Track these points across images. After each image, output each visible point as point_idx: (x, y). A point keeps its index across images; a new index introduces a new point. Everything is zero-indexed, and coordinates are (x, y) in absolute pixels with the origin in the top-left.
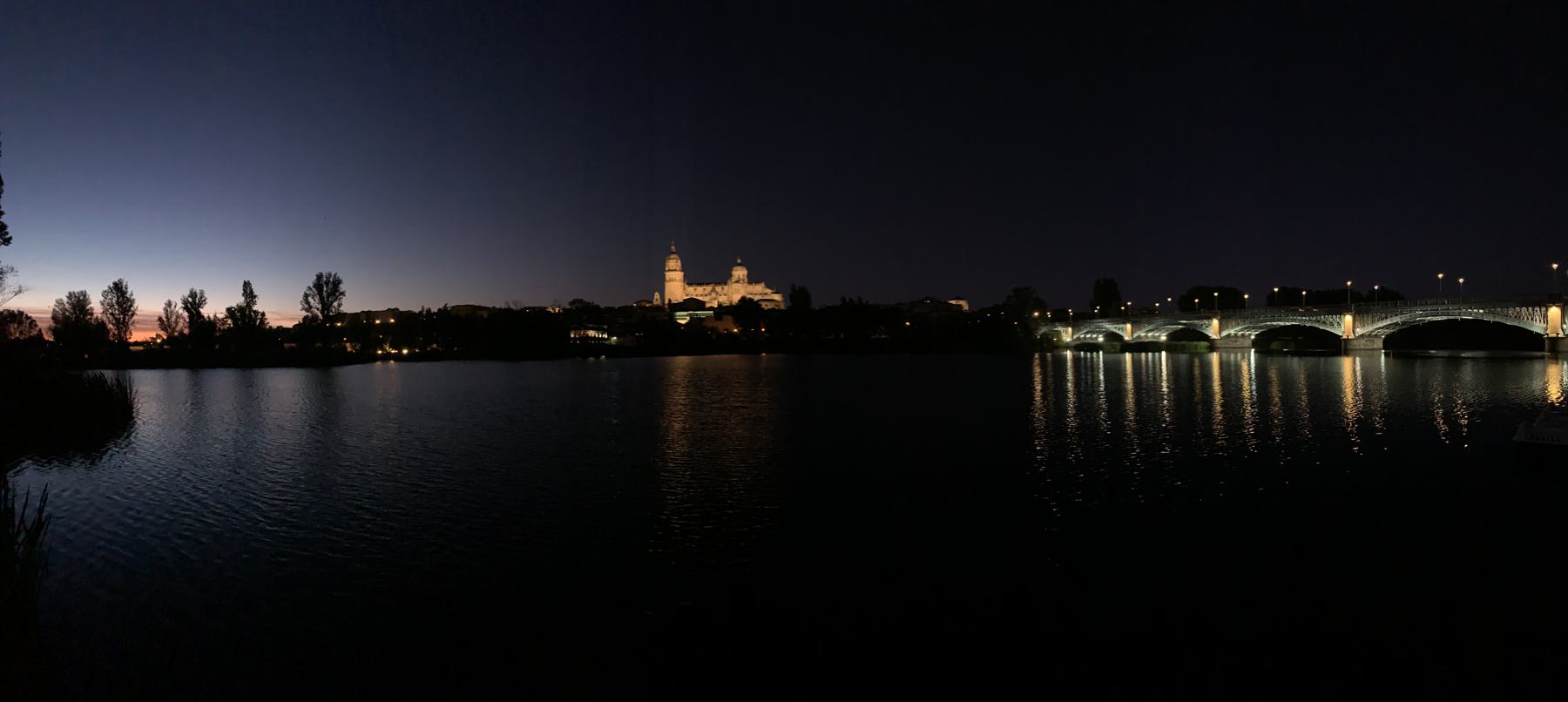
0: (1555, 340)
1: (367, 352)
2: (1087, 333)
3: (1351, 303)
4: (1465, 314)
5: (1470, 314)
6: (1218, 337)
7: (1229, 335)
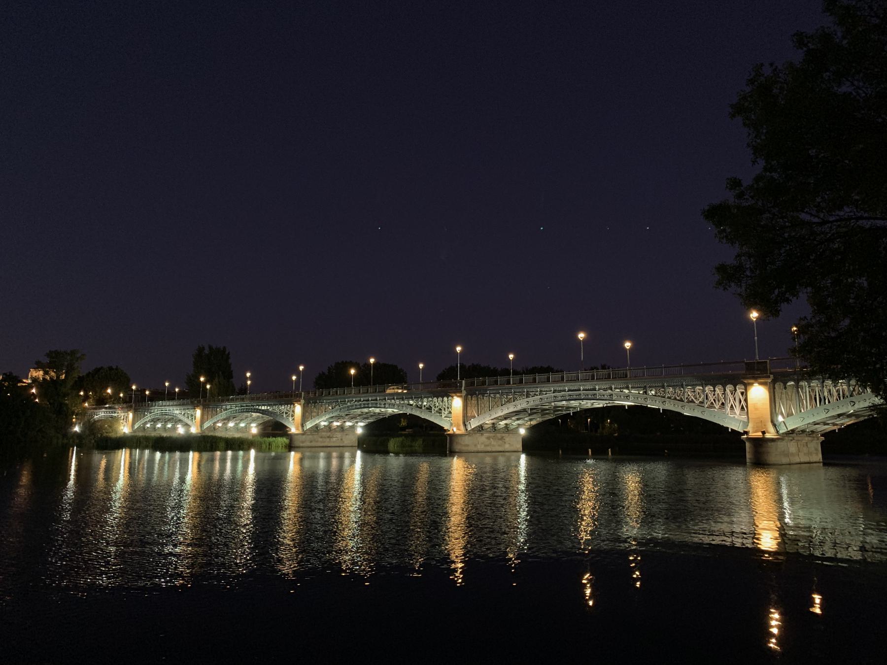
0: (760, 443)
1: (716, 217)
2: (228, 419)
3: (462, 379)
4: (619, 398)
5: (627, 397)
6: (462, 431)
7: (317, 427)
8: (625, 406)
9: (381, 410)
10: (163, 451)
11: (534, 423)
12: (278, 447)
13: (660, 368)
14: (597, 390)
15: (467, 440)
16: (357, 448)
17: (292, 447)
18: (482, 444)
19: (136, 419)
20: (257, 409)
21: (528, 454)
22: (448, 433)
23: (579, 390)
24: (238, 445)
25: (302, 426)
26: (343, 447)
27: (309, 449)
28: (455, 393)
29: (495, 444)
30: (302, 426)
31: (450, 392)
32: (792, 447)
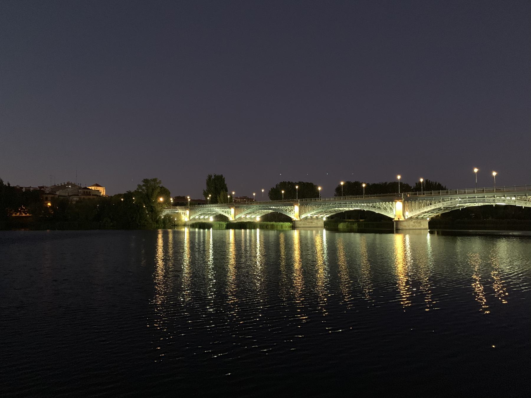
2: (201, 215)
4: (499, 201)
6: (298, 219)
7: (306, 218)
8: (493, 205)
9: (349, 209)
10: (250, 229)
11: (328, 216)
12: (286, 227)
13: (513, 187)
14: (486, 197)
15: (405, 224)
16: (323, 228)
17: (399, 230)
18: (412, 225)
19: (191, 214)
20: (270, 208)
21: (327, 229)
22: (293, 220)
23: (475, 198)
26: (318, 227)
27: (303, 228)
28: (397, 200)
29: (417, 225)
30: (235, 217)
31: (395, 200)
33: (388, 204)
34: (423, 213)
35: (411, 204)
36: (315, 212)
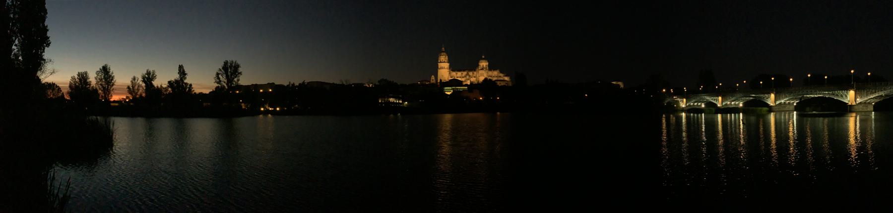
2: (695, 102)
6: (774, 105)
7: (780, 103)
10: (735, 113)
24: (736, 110)
25: (775, 103)
30: (775, 103)
32: (777, 107)
33: (845, 92)
34: (869, 99)
35: (69, 180)
36: (787, 99)
